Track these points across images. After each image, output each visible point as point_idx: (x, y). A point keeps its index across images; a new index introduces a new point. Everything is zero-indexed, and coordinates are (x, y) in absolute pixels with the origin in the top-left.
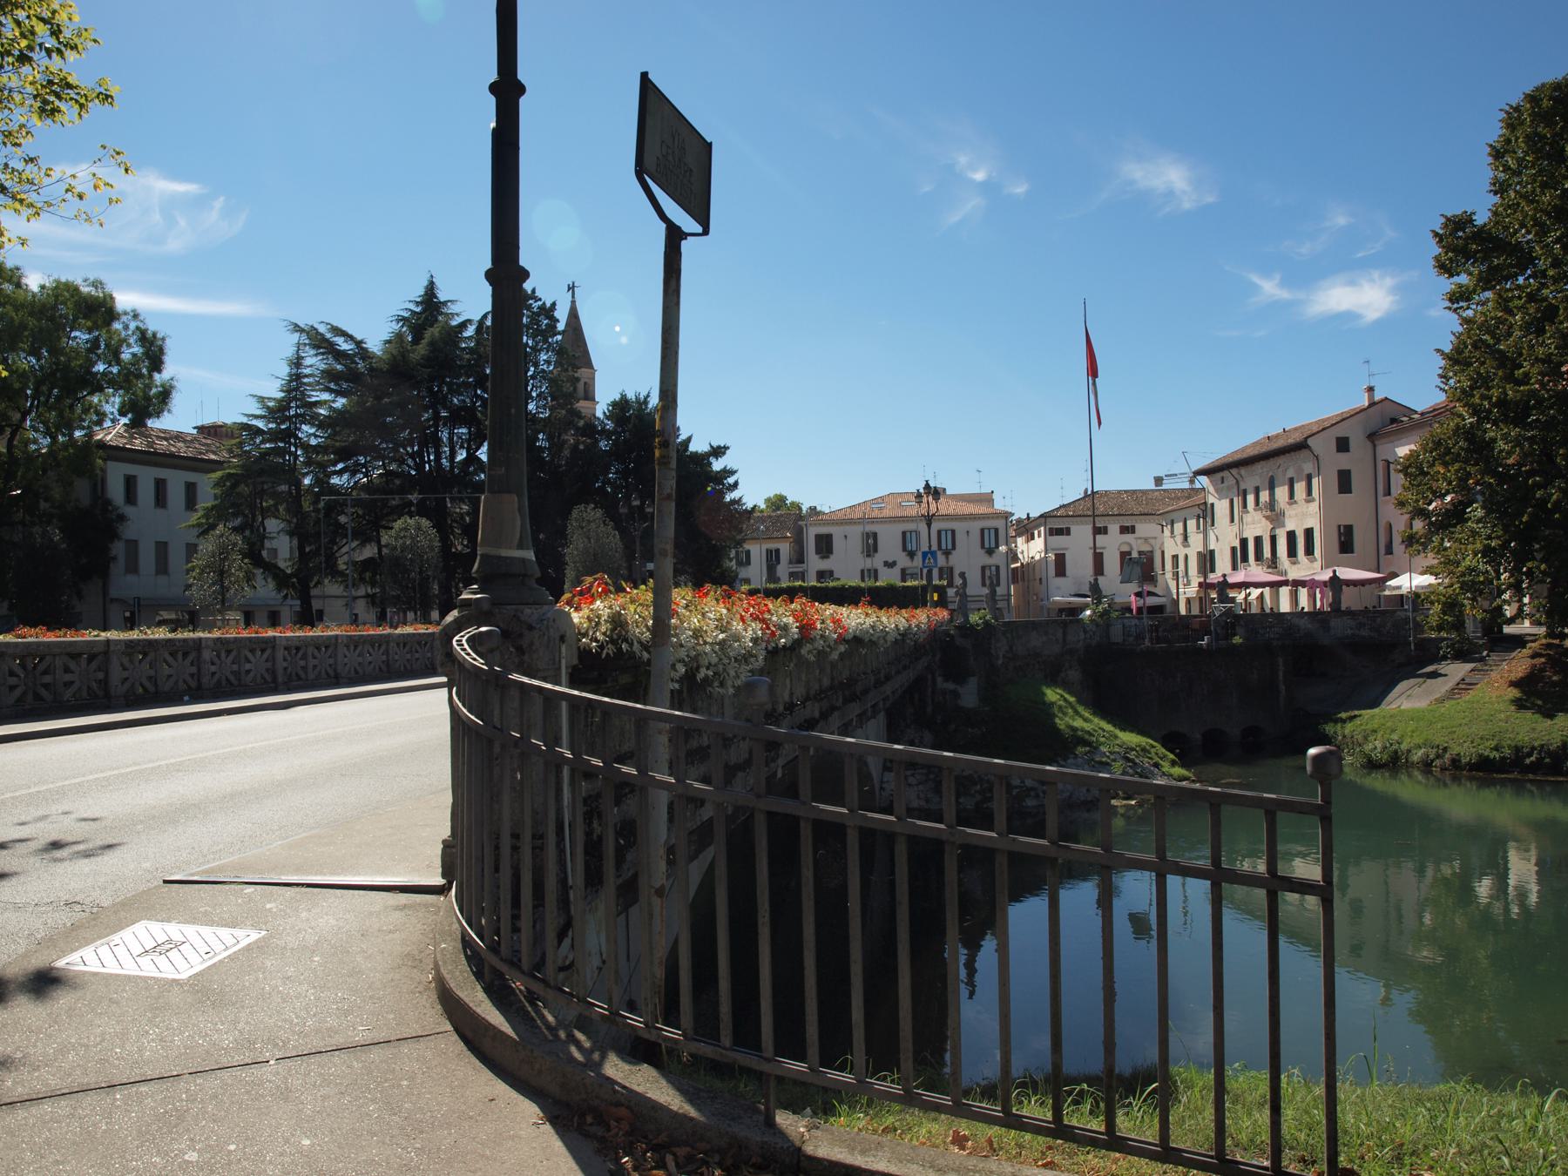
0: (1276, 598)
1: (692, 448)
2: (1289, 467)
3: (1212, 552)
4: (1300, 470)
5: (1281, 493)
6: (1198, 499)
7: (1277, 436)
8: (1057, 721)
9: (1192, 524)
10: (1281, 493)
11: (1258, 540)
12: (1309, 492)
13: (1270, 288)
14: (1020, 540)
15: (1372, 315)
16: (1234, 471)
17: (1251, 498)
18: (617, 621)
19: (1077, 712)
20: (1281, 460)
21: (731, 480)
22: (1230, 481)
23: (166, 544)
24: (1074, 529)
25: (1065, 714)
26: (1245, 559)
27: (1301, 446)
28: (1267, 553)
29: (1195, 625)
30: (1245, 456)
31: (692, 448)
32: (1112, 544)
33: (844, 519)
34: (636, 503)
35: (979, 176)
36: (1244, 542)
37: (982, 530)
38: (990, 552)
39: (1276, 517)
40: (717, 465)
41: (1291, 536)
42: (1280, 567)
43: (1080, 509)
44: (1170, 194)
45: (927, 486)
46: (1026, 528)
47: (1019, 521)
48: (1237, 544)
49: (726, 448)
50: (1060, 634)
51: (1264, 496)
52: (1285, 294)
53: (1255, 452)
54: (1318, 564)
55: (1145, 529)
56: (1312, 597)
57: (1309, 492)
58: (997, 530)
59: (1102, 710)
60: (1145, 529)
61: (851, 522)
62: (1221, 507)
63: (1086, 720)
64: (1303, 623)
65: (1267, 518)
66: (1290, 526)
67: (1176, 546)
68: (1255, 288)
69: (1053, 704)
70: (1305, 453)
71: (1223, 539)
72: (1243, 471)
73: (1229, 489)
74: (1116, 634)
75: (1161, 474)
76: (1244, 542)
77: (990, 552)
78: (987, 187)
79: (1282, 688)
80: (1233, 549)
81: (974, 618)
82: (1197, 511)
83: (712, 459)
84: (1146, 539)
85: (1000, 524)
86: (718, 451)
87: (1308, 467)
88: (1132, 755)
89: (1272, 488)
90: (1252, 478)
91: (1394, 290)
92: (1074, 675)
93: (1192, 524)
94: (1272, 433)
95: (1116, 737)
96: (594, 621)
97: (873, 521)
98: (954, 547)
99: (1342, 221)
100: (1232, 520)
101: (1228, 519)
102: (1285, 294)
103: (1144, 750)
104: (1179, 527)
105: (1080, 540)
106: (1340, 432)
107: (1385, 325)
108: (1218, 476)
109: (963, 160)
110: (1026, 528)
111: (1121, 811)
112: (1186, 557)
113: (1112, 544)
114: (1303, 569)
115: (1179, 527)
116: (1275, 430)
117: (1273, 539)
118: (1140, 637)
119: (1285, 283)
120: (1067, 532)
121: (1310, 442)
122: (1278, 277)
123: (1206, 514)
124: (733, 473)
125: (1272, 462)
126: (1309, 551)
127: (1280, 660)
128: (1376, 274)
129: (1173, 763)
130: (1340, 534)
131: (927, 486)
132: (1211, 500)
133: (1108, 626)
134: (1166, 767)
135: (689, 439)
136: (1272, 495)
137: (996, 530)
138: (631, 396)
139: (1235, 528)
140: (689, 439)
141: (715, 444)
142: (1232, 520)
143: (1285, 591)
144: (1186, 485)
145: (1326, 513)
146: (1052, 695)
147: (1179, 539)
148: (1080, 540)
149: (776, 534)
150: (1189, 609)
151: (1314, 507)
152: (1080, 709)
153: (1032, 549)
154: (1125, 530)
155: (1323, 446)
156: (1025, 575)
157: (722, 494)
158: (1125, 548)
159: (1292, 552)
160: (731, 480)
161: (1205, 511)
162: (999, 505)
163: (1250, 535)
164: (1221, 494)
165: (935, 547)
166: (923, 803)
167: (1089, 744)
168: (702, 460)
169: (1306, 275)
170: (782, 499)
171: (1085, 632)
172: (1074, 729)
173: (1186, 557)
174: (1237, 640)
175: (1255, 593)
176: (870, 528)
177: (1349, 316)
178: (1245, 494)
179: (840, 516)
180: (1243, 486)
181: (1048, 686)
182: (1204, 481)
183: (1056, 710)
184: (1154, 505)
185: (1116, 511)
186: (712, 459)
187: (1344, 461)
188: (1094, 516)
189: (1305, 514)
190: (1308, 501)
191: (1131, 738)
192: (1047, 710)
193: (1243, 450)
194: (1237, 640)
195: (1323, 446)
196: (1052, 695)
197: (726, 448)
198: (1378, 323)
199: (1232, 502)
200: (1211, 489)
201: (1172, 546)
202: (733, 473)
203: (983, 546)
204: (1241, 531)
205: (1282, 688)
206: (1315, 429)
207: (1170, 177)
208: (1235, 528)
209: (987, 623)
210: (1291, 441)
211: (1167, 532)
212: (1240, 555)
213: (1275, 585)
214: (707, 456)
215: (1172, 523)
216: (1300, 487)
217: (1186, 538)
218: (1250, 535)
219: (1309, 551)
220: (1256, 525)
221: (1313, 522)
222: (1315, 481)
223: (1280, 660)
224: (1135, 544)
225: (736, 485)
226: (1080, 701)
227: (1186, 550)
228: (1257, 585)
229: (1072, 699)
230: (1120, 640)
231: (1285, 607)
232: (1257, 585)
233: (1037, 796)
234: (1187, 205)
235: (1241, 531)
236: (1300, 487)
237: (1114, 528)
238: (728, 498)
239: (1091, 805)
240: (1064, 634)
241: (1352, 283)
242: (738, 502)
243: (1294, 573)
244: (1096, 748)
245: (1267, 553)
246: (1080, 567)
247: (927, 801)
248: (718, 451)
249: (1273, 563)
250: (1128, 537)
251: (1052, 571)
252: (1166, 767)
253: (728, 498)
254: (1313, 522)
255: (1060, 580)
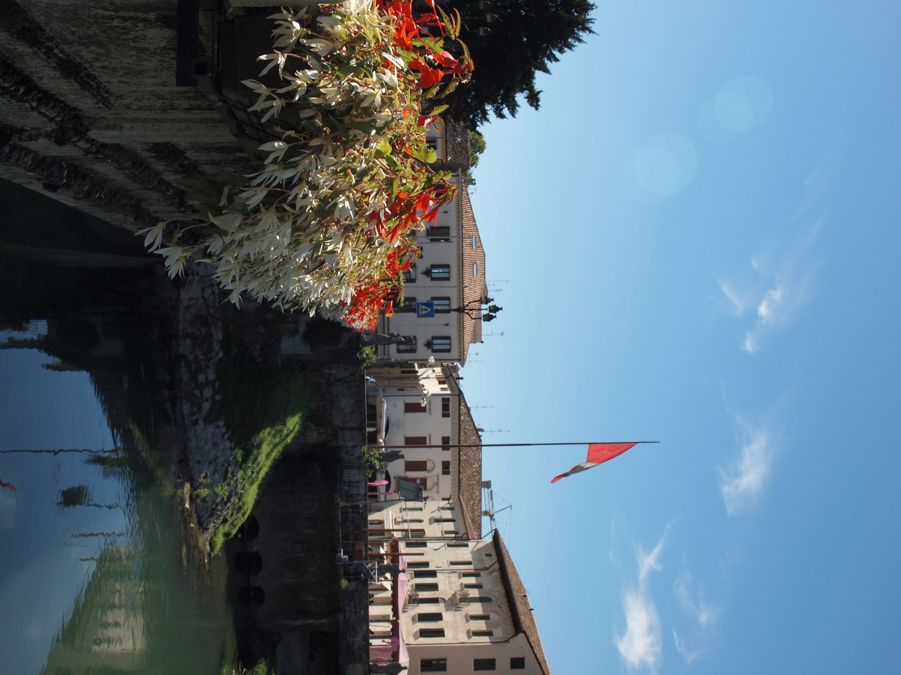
0: (383, 602)
1: (538, 74)
2: (500, 615)
3: (424, 545)
4: (496, 625)
5: (476, 608)
6: (473, 533)
7: (526, 603)
8: (268, 430)
9: (450, 526)
10: (476, 608)
11: (434, 587)
12: (477, 634)
13: (649, 562)
14: (438, 370)
15: (622, 647)
16: (497, 566)
17: (472, 580)
18: (349, 121)
19: (276, 446)
20: (505, 608)
21: (506, 111)
22: (488, 562)
23: (475, 661)
24: (448, 420)
25: (274, 436)
26: (418, 574)
27: (517, 627)
28: (423, 595)
29: (359, 546)
30: (510, 576)
31: (538, 74)
32: (435, 457)
33: (462, 210)
34: (489, 18)
35: (763, 310)
36: (433, 574)
37: (448, 338)
38: (429, 345)
39: (454, 603)
40: (521, 98)
41: (437, 617)
42: (410, 607)
43: (466, 426)
44: (737, 475)
45: (495, 309)
46: (450, 377)
47: (456, 369)
48: (432, 567)
49: (537, 107)
50: (351, 424)
51: (474, 593)
52: (643, 574)
53: (514, 586)
54: (411, 641)
55: (447, 484)
56: (382, 636)
57: (477, 634)
58: (449, 353)
59: (277, 466)
60: (447, 484)
61: (460, 217)
62: (464, 554)
63: (268, 455)
64: (358, 640)
65: (454, 595)
66: (446, 616)
67: (429, 515)
68: (649, 549)
69: (284, 424)
70: (511, 630)
71: (437, 555)
72: (496, 574)
73: (481, 561)
74: (351, 475)
75: (493, 487)
76: (433, 574)
77: (429, 345)
78: (753, 315)
79: (299, 623)
80: (426, 564)
81: (367, 350)
82: (462, 532)
83: (526, 93)
84: (437, 484)
85: (454, 354)
86: (534, 99)
87: (498, 633)
88: (234, 499)
89: (481, 600)
90: (490, 581)
91: (644, 664)
92: (313, 437)
93: (450, 526)
94: (530, 599)
95: (252, 483)
96: (351, 57)
97: (461, 238)
98: (433, 279)
99: (704, 618)
100: (452, 563)
101: (453, 559)
102: (643, 574)
103: (240, 508)
104: (448, 514)
105: (436, 427)
106: (529, 660)
107: (614, 655)
108: (493, 551)
109: (777, 295)
110: (450, 377)
111: (179, 492)
112: (421, 521)
113: (435, 457)
114: (408, 628)
115: (448, 514)
116: (532, 601)
117: (435, 601)
118: (349, 497)
119: (653, 575)
120: (446, 414)
121: (521, 635)
122: (659, 568)
123: (459, 540)
124: (513, 113)
125: (503, 601)
126: (424, 633)
127: (325, 621)
128: (658, 649)
129: (226, 535)
130: (438, 660)
131: (495, 309)
132: (472, 544)
133: (359, 468)
134: (222, 529)
135: (547, 71)
136: (474, 600)
137: (448, 351)
138: (591, 14)
139: (445, 566)
140: (547, 71)
141: (540, 96)
142: (452, 563)
143: (387, 610)
144: (483, 509)
145: (460, 649)
146: (293, 423)
147: (437, 515)
148: (436, 427)
149: (450, 146)
150: (373, 523)
151: (463, 638)
152: (280, 448)
153: (431, 383)
154: (446, 466)
155: (517, 646)
156: (408, 374)
157: (493, 102)
158: (429, 466)
159: (423, 617)
160: (506, 111)
161: (461, 538)
162: (472, 349)
163: (440, 580)
164: (476, 553)
165: (435, 308)
166: (185, 303)
167: (245, 459)
168: (526, 83)
169: (660, 593)
170: (481, 149)
171: (353, 447)
172: (259, 446)
173: (421, 521)
174: (344, 583)
175: (388, 585)
176: (453, 232)
177: (622, 627)
178: (476, 575)
179: (465, 207)
180: (482, 573)
181: (302, 418)
182: (489, 539)
183: (279, 427)
184: (469, 489)
185: (463, 458)
186: (526, 93)
187: (503, 664)
188: (459, 447)
189: (457, 630)
190: (468, 632)
191: (251, 495)
192: (278, 419)
193: (515, 573)
194: (344, 583)
195: (517, 646)
196: (293, 423)
197: (537, 107)
198: (615, 652)
199: (469, 563)
200: (481, 545)
201: (432, 507)
202: (513, 113)
203: (434, 338)
204: (443, 571)
205: (299, 623)
206: (532, 639)
207: (751, 473)
208: (445, 566)
209: (363, 360)
210: (522, 618)
211: (444, 504)
212: (422, 570)
213: (394, 601)
214: (530, 88)
215: (451, 509)
216: (481, 625)
217: (438, 521)
218: (440, 580)
219: (424, 633)
220: (448, 585)
221: (450, 638)
222: (486, 639)
223: (325, 621)
224: (434, 474)
225: (501, 116)
226: (287, 447)
227: (426, 521)
228: (395, 588)
229: (289, 440)
230: (346, 478)
231: (374, 611)
232: (395, 588)
233: (193, 414)
234: (726, 490)
235: (443, 571)
236: (481, 625)
237: (448, 456)
238: (488, 107)
239: (184, 461)
240: (351, 429)
241: (651, 629)
242: (484, 118)
243: (405, 620)
244: (241, 467)
245: (423, 595)
246: (415, 425)
247: (187, 308)
248: (534, 99)
249: (413, 600)
250: (439, 469)
251: (410, 400)
252: (222, 529)
253: (488, 107)
254: (450, 638)
255: (402, 407)
